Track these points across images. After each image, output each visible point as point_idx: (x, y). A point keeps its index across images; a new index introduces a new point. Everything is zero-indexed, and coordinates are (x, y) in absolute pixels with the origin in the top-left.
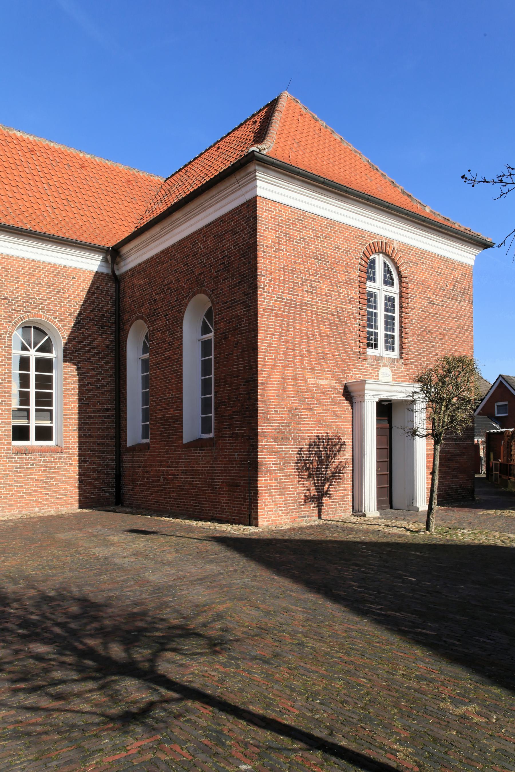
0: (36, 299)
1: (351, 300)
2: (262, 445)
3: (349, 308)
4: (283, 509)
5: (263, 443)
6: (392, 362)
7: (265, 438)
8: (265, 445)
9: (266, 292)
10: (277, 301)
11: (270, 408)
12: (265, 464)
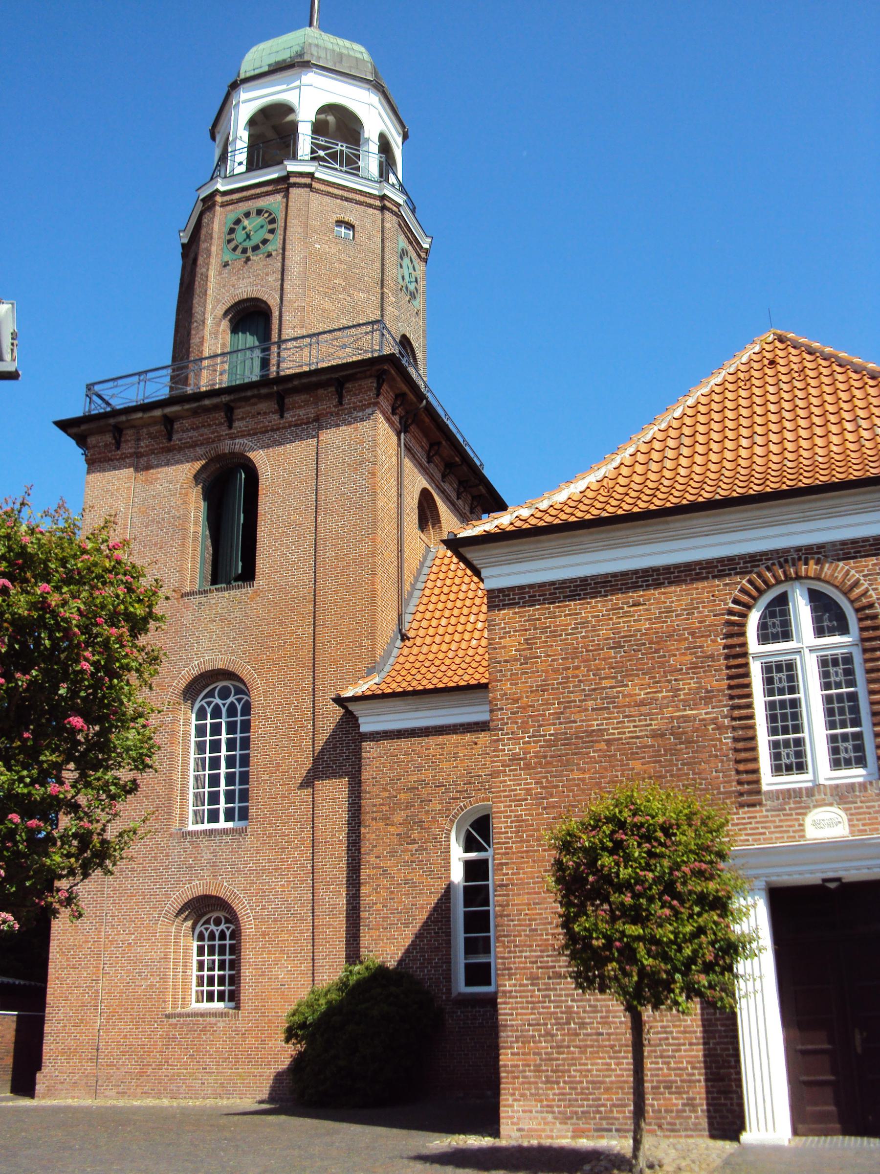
0: (481, 776)
1: (708, 698)
2: (504, 992)
3: (703, 712)
4: (556, 1109)
5: (508, 988)
6: (842, 795)
7: (510, 979)
8: (511, 991)
9: (507, 734)
10: (529, 743)
11: (520, 925)
12: (512, 1026)
